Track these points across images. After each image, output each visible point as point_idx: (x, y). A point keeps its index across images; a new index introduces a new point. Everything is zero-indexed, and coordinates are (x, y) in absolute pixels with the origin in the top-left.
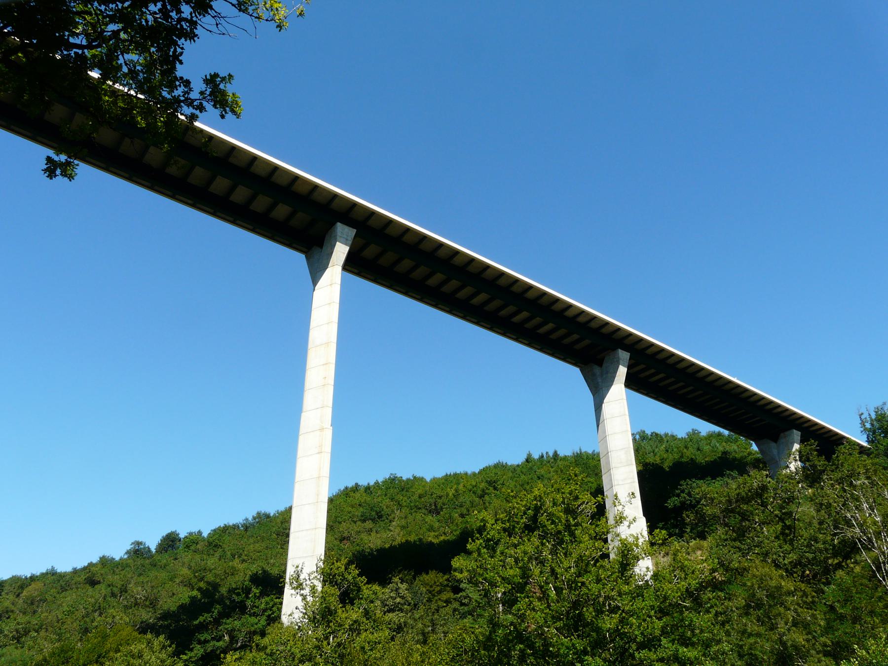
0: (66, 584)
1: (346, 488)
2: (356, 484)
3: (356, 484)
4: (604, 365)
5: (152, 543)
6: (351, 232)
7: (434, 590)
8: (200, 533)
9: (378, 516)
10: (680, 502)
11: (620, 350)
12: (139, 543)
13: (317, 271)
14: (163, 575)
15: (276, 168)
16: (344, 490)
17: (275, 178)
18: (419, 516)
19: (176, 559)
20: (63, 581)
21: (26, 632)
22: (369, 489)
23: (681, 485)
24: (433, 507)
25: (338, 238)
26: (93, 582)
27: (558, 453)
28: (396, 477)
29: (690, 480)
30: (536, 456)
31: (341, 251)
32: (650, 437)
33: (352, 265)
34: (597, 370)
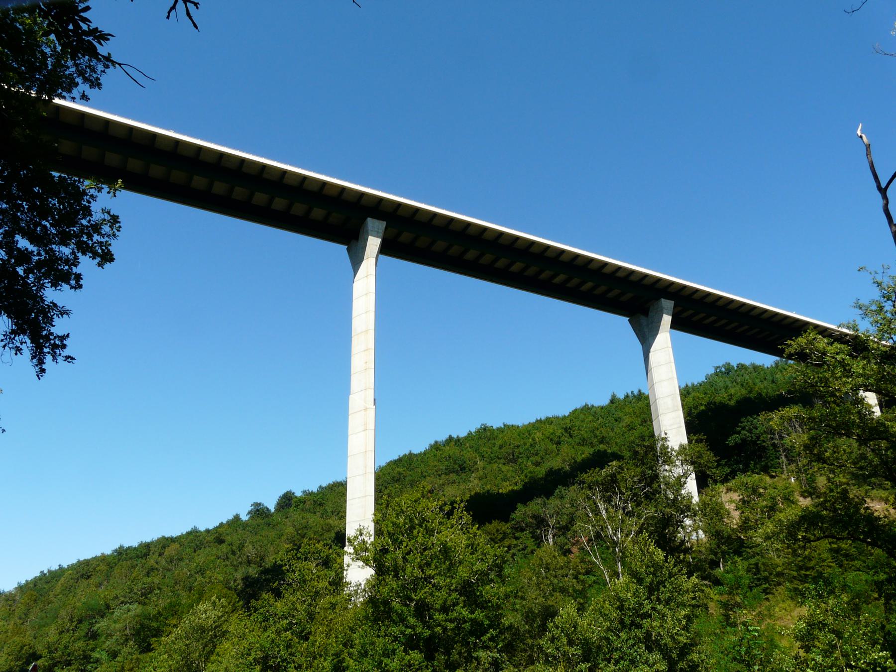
1: (436, 442)
3: (450, 436)
4: (650, 314)
5: (271, 504)
6: (381, 225)
7: (496, 538)
8: (237, 518)
9: (461, 468)
10: (742, 439)
11: (663, 300)
12: (257, 504)
13: (356, 260)
14: (272, 534)
15: (305, 178)
18: (495, 466)
19: (287, 518)
21: (151, 590)
23: (742, 422)
24: (512, 457)
25: (369, 232)
26: (220, 541)
27: (642, 392)
28: (487, 427)
29: (751, 417)
30: (621, 396)
31: (373, 243)
32: (736, 368)
33: (386, 249)
34: (643, 320)
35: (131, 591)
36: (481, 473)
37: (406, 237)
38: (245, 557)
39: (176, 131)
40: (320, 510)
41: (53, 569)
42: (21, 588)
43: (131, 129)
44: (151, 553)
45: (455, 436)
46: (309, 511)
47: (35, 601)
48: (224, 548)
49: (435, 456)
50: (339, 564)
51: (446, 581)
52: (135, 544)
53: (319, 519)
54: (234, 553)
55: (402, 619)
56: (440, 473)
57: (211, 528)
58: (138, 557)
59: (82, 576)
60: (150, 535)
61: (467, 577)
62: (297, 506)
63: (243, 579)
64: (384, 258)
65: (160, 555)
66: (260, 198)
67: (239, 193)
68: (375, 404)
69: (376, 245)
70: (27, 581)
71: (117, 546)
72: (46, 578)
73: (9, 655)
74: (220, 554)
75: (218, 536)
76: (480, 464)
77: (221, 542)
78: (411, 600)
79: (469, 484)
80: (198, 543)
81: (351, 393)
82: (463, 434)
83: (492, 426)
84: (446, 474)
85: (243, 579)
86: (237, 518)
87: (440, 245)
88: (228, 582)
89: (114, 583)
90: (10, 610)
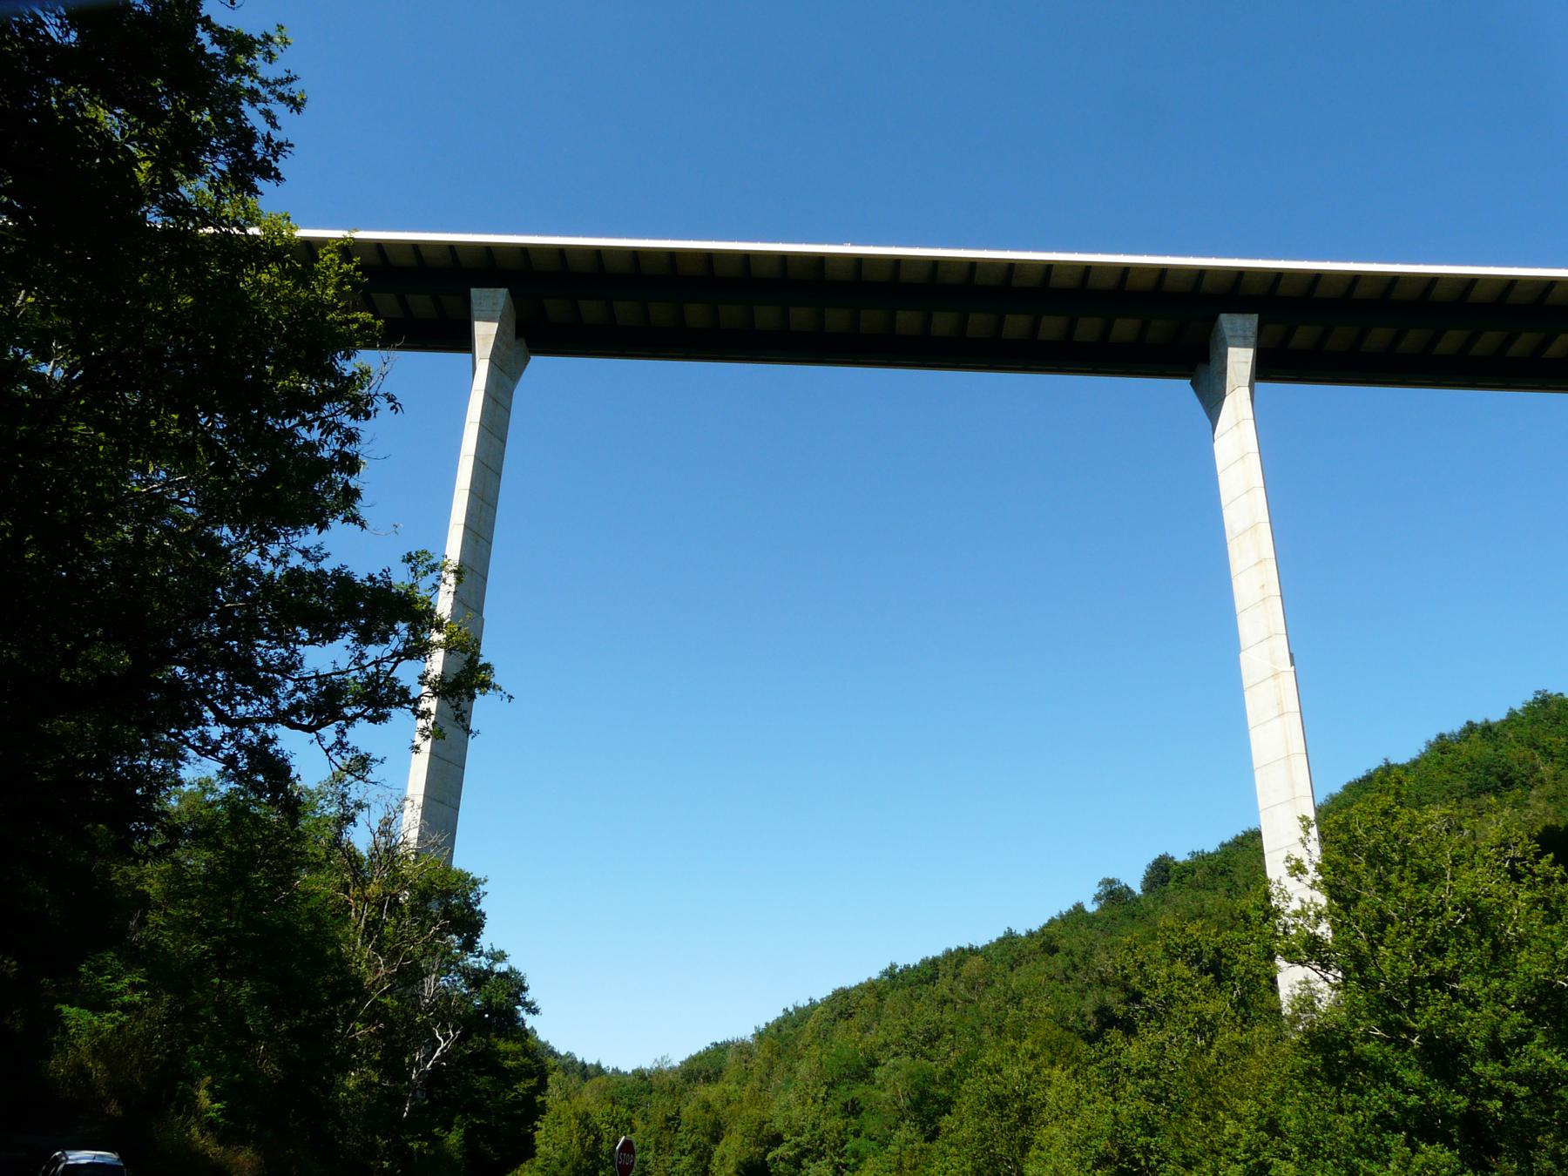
0: (1019, 955)
1: (1441, 736)
2: (1469, 723)
3: (1469, 723)
5: (1134, 880)
6: (500, 296)
8: (1079, 908)
12: (1110, 882)
13: (1212, 400)
16: (1436, 740)
17: (1055, 282)
20: (1015, 951)
22: (1490, 730)
25: (1229, 343)
31: (1240, 361)
33: (1264, 370)
35: (909, 1033)
36: (1550, 788)
37: (1304, 336)
38: (1096, 975)
39: (854, 243)
40: (1223, 884)
41: (801, 1005)
42: (760, 1036)
43: (784, 258)
44: (940, 975)
45: (1478, 720)
46: (1204, 887)
47: (779, 1055)
48: (1060, 960)
49: (1439, 763)
50: (1243, 964)
51: (1491, 986)
52: (914, 960)
53: (1223, 899)
54: (1075, 968)
55: (1381, 1073)
56: (1458, 795)
57: (1035, 928)
58: (921, 981)
59: (840, 1014)
60: (935, 949)
61: (1546, 974)
62: (1180, 879)
63: (1095, 1013)
64: (1263, 387)
65: (955, 977)
66: (1016, 325)
67: (978, 323)
68: (1292, 663)
69: (1247, 362)
70: (767, 1024)
71: (885, 966)
72: (793, 1020)
73: (745, 1136)
74: (1052, 970)
75: (1047, 942)
76: (1546, 770)
77: (1053, 950)
78: (1412, 1032)
79: (1526, 811)
80: (1015, 955)
81: (1243, 648)
82: (1497, 715)
83: (1561, 694)
84: (1471, 795)
85: (1095, 1013)
86: (1079, 908)
87: (1379, 337)
88: (1064, 1019)
89: (887, 1026)
90: (746, 1069)
